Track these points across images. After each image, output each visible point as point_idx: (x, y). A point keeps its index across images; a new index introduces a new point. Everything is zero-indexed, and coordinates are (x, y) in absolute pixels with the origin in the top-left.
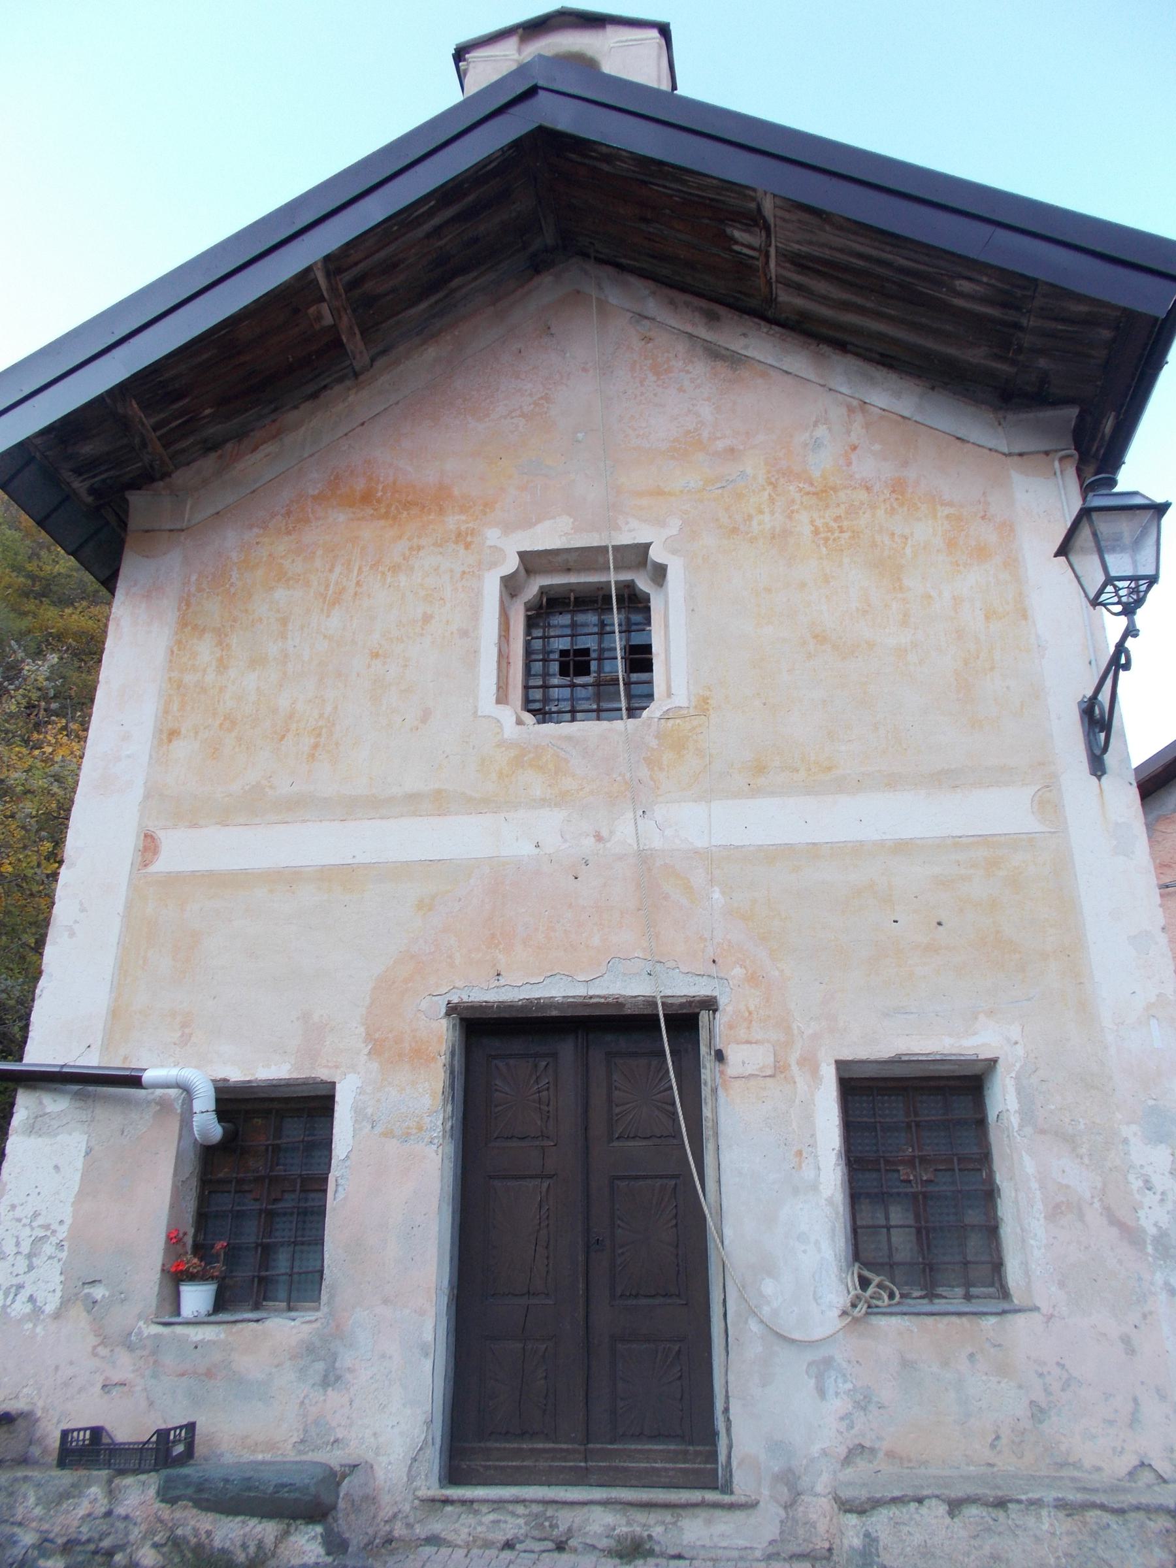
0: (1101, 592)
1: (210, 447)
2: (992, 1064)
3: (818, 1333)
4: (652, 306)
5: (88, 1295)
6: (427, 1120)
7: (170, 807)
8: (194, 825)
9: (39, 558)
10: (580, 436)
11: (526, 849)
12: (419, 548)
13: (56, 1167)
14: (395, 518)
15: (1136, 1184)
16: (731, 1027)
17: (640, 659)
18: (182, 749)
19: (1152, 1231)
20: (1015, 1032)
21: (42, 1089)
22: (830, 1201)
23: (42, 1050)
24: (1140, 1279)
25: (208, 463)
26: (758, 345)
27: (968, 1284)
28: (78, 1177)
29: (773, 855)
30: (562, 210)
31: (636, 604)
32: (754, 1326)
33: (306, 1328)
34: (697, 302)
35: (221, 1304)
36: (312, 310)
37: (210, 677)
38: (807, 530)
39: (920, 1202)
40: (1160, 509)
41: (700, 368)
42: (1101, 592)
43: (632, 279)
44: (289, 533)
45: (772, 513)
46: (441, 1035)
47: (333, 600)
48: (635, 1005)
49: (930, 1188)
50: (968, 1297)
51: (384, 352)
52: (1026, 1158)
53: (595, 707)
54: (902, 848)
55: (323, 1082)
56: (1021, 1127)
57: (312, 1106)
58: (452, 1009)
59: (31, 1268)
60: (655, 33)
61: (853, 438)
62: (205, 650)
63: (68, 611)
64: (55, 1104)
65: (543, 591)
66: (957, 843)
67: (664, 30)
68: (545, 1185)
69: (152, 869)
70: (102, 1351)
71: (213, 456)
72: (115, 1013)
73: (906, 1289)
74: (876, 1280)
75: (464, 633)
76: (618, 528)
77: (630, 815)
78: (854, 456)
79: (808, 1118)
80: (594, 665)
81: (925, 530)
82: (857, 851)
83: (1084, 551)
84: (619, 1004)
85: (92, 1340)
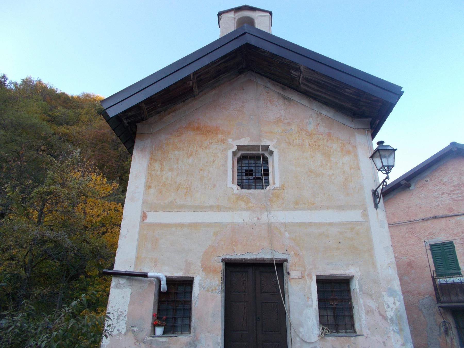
0: (381, 168)
1: (158, 113)
2: (352, 277)
3: (313, 340)
4: (269, 85)
5: (133, 329)
6: (217, 287)
7: (148, 206)
8: (156, 211)
9: (52, 110)
10: (251, 116)
11: (240, 221)
12: (212, 143)
13: (123, 297)
14: (205, 135)
15: (386, 306)
16: (291, 266)
17: (266, 173)
18: (152, 191)
19: (390, 317)
20: (358, 269)
21: (119, 277)
22: (315, 309)
23: (117, 268)
24: (387, 328)
25: (157, 117)
26: (295, 97)
27: (346, 329)
28: (129, 300)
29: (301, 225)
30: (249, 61)
31: (266, 160)
32: (298, 339)
33: (189, 338)
34: (280, 85)
35: (165, 332)
36: (188, 83)
37: (159, 173)
38: (307, 144)
39: (334, 309)
40: (395, 150)
41: (281, 101)
42: (381, 168)
43: (264, 78)
44: (178, 136)
45: (299, 140)
46: (220, 266)
47: (190, 155)
48: (268, 260)
49: (337, 306)
50: (346, 332)
51: (202, 91)
52: (361, 299)
53: (254, 185)
54: (331, 224)
55: (191, 277)
56: (359, 292)
57: (187, 283)
58: (223, 260)
59: (118, 322)
60: (268, 14)
61: (318, 122)
62: (157, 166)
63: (61, 127)
64: (122, 281)
65: (242, 155)
66: (343, 223)
67: (271, 13)
68: (245, 304)
69: (145, 222)
70: (137, 343)
71: (158, 115)
72: (137, 258)
73: (332, 330)
74: (326, 328)
75: (223, 165)
76: (261, 141)
77: (266, 213)
78: (318, 127)
79: (310, 289)
80: (254, 174)
81: (336, 146)
82: (320, 225)
83: (377, 158)
84: (264, 260)
85: (134, 341)
